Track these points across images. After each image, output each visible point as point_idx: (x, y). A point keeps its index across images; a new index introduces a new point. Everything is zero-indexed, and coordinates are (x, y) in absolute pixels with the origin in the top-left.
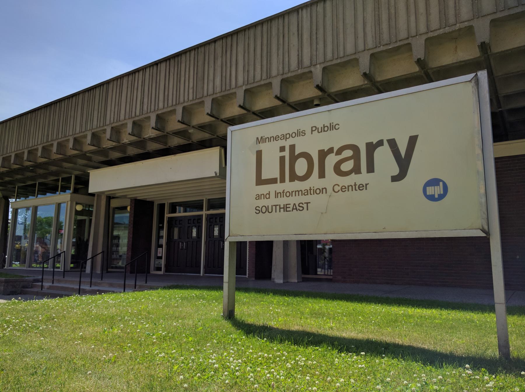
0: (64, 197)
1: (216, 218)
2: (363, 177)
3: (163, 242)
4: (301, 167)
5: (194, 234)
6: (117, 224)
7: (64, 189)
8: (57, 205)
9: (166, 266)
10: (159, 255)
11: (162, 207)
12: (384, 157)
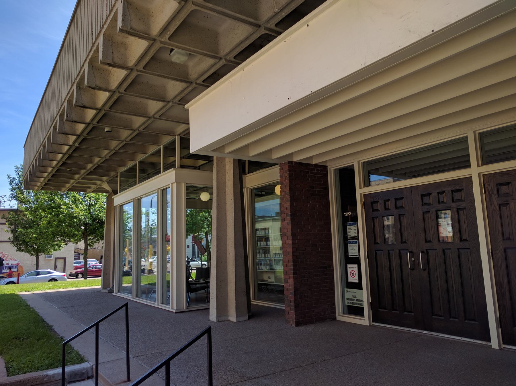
0: (167, 178)
1: (386, 201)
3: (360, 249)
5: (446, 229)
6: (259, 217)
7: (169, 166)
8: (160, 192)
9: (373, 306)
10: (353, 279)
11: (346, 175)
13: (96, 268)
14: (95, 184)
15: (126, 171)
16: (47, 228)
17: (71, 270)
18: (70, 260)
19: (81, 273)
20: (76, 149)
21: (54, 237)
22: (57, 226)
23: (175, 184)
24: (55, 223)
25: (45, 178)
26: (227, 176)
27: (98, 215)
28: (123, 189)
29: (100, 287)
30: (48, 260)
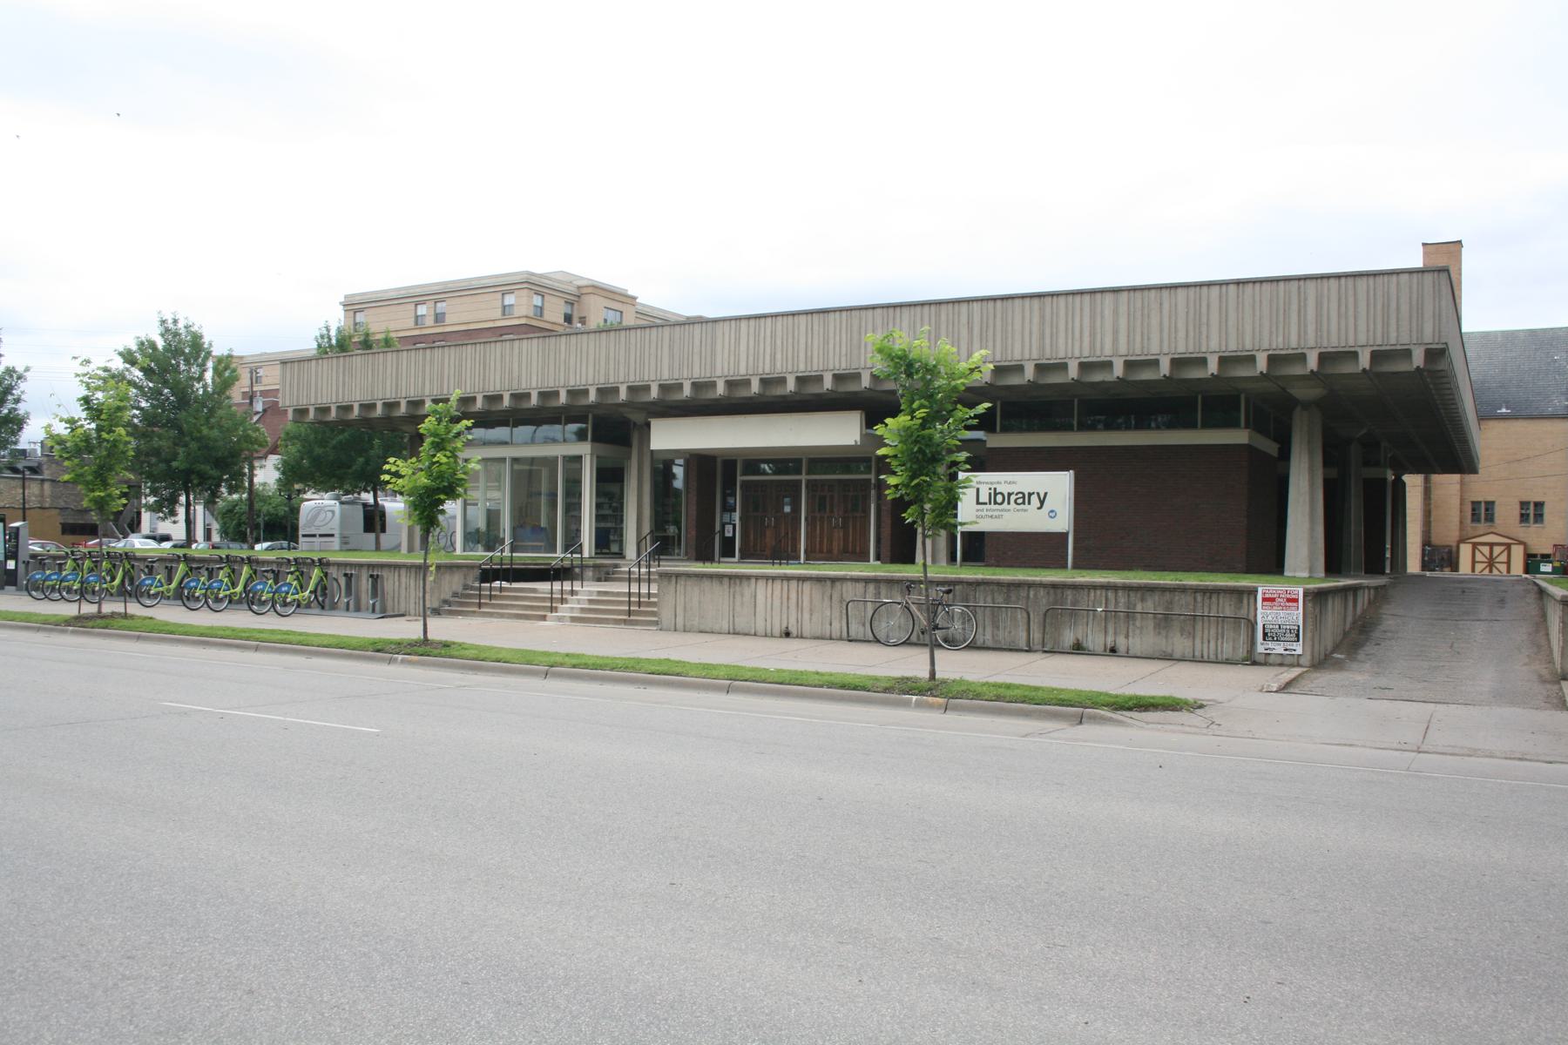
2: (1026, 506)
4: (999, 498)
5: (787, 509)
12: (1035, 500)
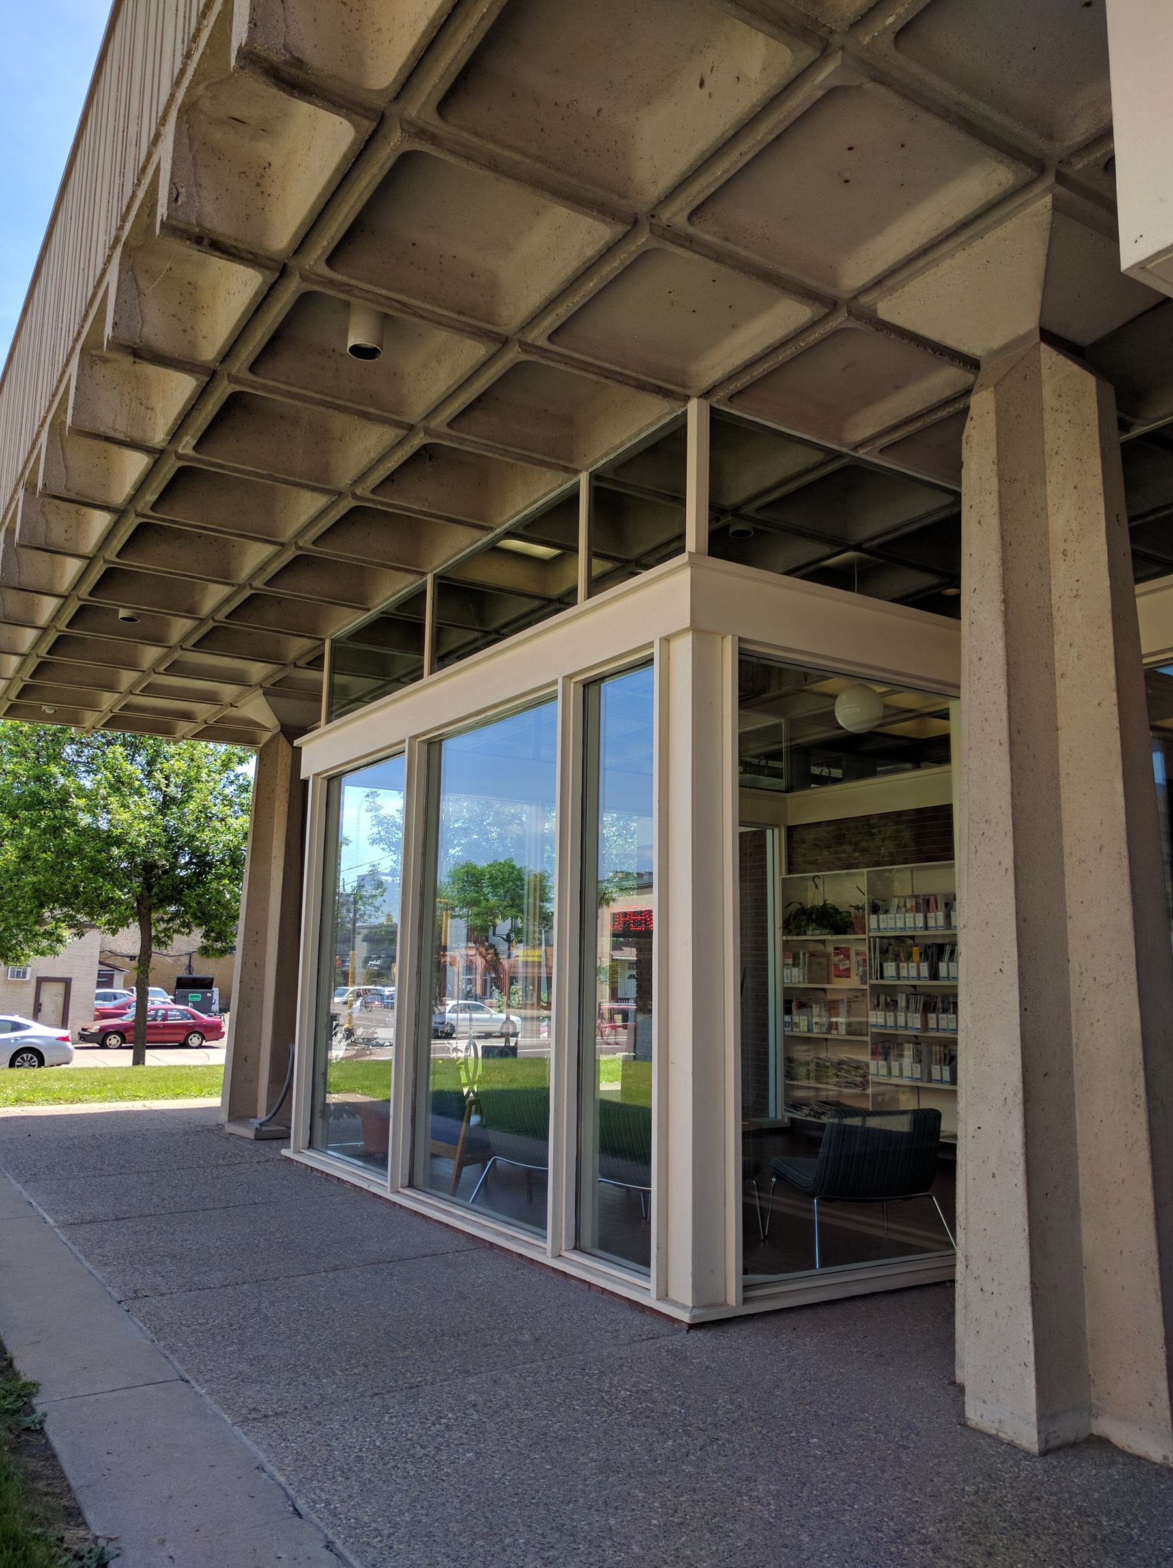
13: (165, 1017)
14: (210, 698)
15: (358, 635)
16: (19, 873)
17: (83, 1019)
18: (85, 987)
19: (121, 1032)
20: (185, 478)
21: (42, 906)
22: (53, 868)
23: (688, 638)
24: (49, 856)
25: (25, 656)
26: (1060, 571)
27: (192, 838)
28: (344, 703)
29: (216, 1101)
30: (15, 983)
